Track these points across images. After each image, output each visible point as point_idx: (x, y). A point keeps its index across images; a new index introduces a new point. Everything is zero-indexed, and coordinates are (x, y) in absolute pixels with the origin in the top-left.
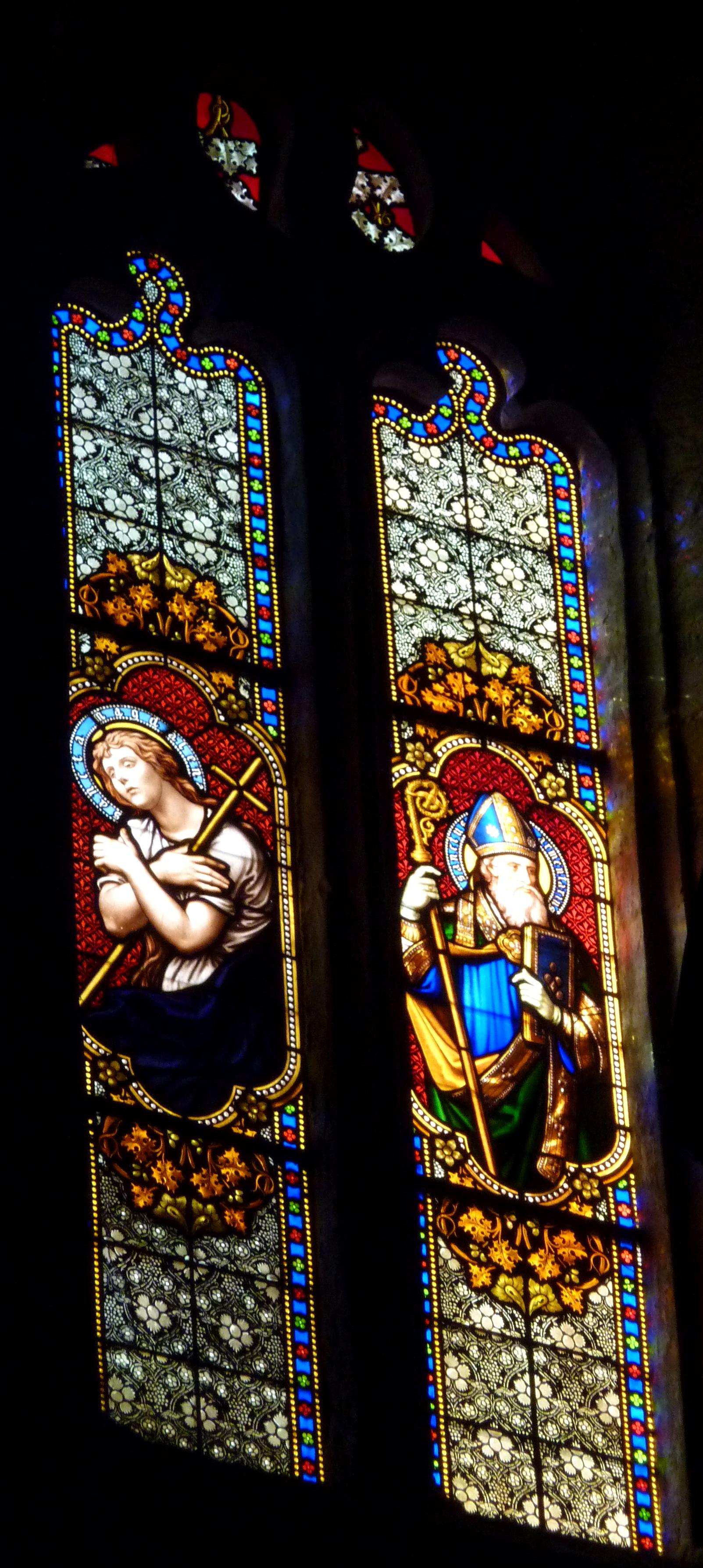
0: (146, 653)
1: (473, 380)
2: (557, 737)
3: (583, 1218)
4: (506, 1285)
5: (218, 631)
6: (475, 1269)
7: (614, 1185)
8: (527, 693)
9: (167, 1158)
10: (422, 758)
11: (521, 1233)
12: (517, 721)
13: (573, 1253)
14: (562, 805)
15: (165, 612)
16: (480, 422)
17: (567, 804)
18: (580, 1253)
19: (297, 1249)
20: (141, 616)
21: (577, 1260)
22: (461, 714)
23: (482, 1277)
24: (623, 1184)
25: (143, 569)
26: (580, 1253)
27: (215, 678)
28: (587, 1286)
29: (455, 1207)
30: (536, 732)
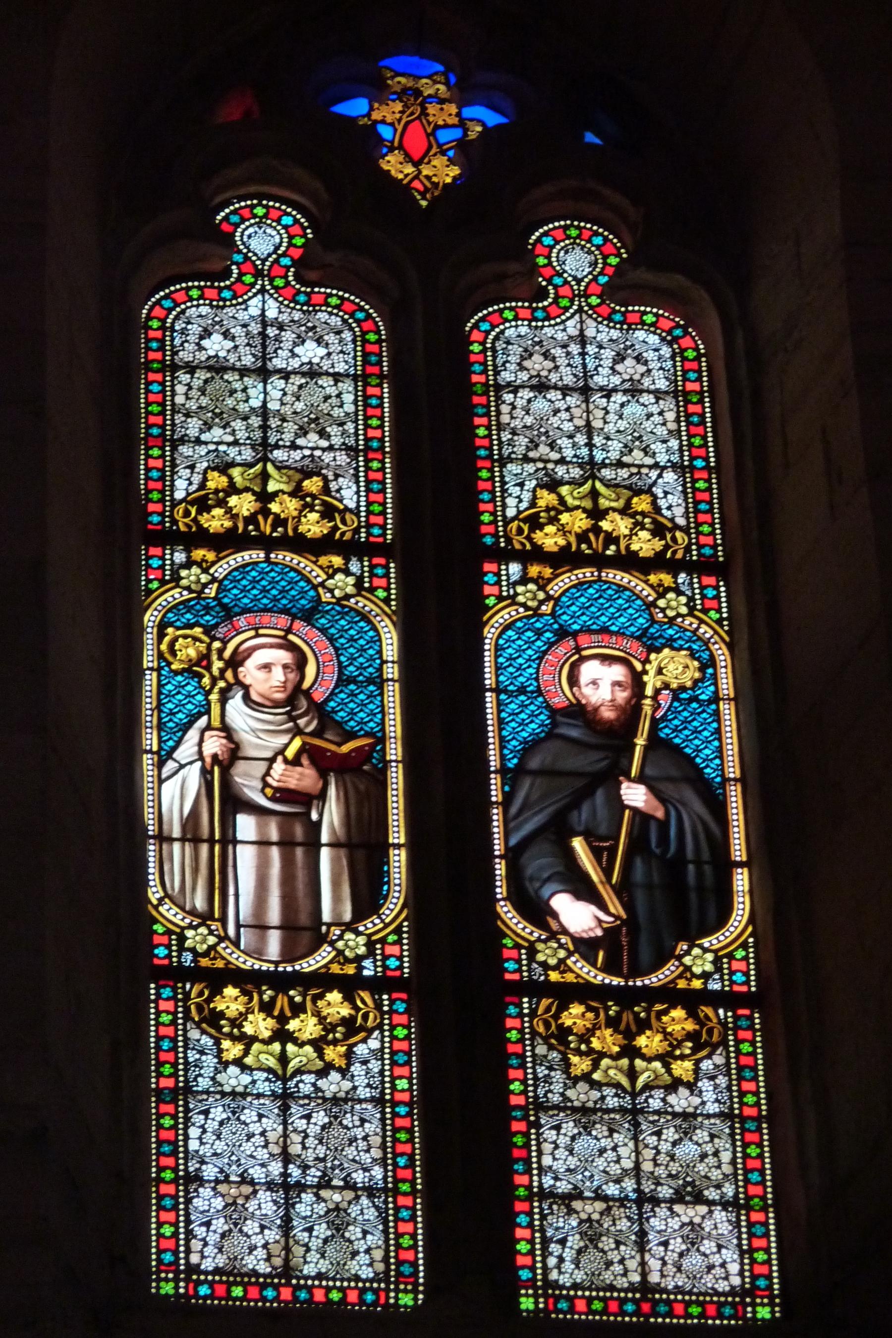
0: (584, 570)
1: (286, 227)
2: (679, 555)
3: (695, 991)
4: (609, 1068)
5: (654, 537)
6: (575, 1059)
7: (731, 956)
8: (317, 502)
9: (608, 1026)
10: (534, 598)
11: (627, 1017)
12: (634, 547)
13: (338, 1013)
14: (353, 600)
15: (266, 512)
16: (288, 283)
17: (359, 598)
18: (690, 1026)
19: (748, 1086)
20: (572, 539)
21: (343, 1019)
22: (574, 549)
23: (580, 1065)
24: (740, 954)
25: (574, 498)
26: (690, 1026)
27: (653, 578)
28: (353, 1040)
29: (206, 993)
30: (656, 554)
